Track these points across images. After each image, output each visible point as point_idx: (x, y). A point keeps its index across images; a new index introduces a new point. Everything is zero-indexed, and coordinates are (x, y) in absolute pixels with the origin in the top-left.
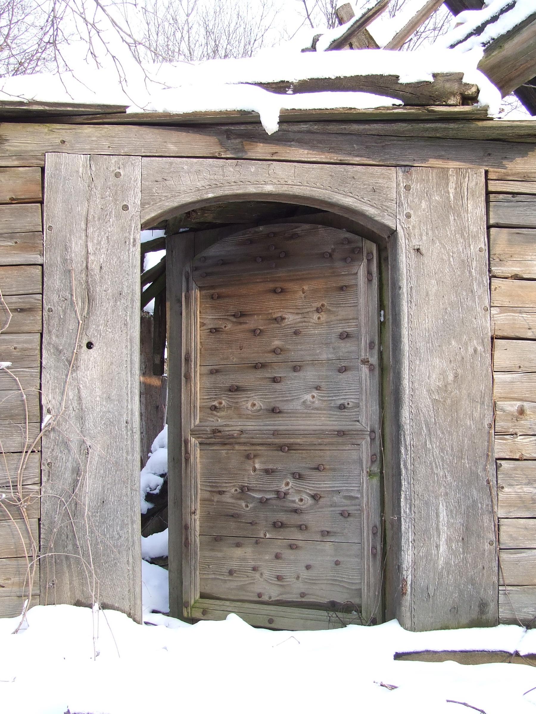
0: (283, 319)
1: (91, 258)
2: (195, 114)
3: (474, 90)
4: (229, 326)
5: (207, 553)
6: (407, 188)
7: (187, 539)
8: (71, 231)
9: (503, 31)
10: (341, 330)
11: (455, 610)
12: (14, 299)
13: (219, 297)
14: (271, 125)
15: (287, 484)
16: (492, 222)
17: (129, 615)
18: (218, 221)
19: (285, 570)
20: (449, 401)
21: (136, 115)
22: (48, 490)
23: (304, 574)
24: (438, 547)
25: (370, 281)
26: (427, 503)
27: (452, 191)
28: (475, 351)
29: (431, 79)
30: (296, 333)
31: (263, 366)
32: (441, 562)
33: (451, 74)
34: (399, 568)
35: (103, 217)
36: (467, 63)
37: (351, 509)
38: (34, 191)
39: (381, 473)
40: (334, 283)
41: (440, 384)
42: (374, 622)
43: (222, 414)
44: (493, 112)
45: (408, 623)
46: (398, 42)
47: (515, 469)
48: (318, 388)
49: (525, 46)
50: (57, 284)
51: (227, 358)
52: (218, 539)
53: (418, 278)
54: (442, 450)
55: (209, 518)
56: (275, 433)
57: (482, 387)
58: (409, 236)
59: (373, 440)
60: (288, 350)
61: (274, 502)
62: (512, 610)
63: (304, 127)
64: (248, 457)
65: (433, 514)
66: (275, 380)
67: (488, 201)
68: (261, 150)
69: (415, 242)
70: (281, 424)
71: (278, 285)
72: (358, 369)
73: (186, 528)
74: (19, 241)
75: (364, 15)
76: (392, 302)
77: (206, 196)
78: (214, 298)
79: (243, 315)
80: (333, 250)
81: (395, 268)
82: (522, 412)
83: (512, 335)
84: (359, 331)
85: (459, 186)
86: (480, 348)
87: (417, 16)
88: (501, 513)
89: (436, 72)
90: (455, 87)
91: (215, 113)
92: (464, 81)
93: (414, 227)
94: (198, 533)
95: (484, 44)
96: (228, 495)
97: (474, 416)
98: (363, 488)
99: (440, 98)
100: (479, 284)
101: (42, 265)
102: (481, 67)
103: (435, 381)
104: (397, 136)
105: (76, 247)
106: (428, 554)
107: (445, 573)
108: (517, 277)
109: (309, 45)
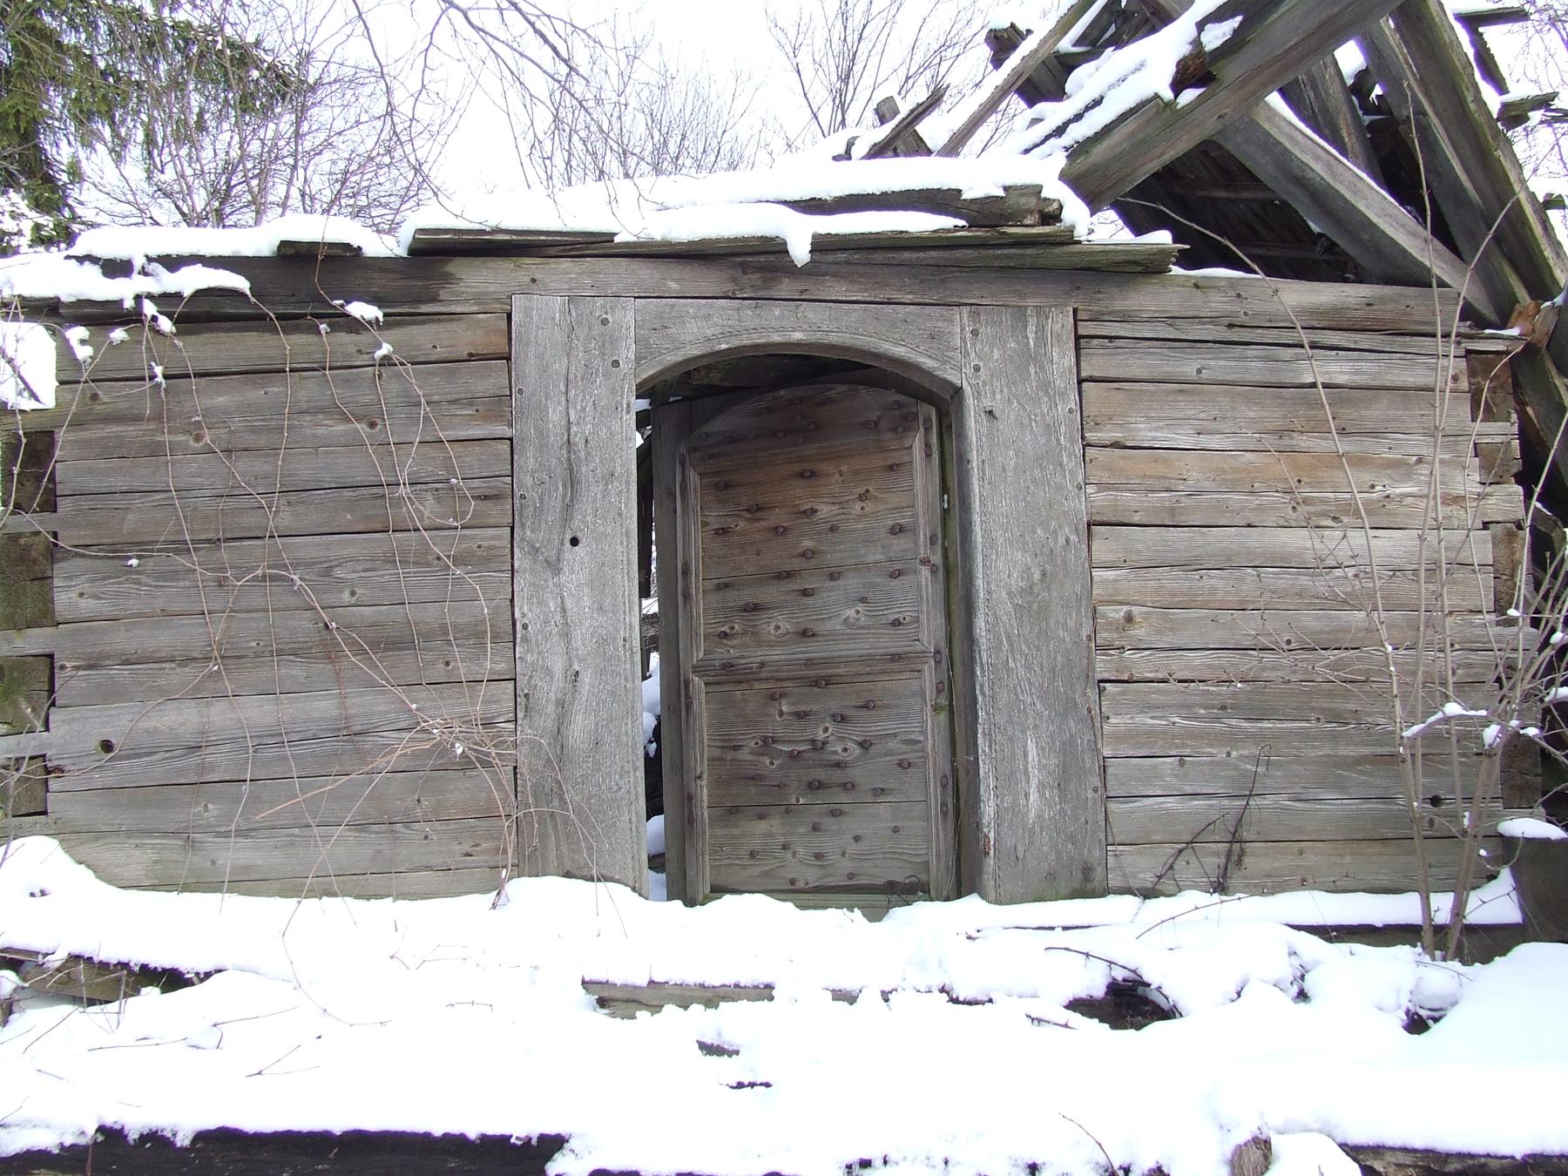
0: (814, 511)
1: (574, 428)
2: (703, 242)
3: (1055, 206)
4: (742, 524)
5: (719, 832)
6: (975, 333)
7: (691, 812)
8: (547, 396)
9: (1090, 133)
10: (890, 523)
11: (1051, 877)
12: (476, 483)
13: (727, 486)
14: (800, 252)
15: (826, 730)
16: (1083, 374)
17: (634, 889)
18: (726, 384)
19: (827, 844)
20: (1035, 606)
21: (627, 244)
22: (526, 732)
23: (852, 848)
24: (1027, 795)
25: (928, 456)
26: (1011, 739)
27: (1031, 336)
28: (1067, 541)
29: (1001, 193)
30: (833, 529)
31: (789, 575)
32: (1032, 815)
33: (1027, 187)
34: (978, 825)
35: (589, 373)
36: (1045, 173)
37: (911, 756)
38: (499, 343)
39: (951, 705)
40: (879, 461)
41: (1023, 584)
42: (947, 899)
43: (736, 642)
44: (1081, 233)
45: (992, 895)
46: (954, 146)
47: (1122, 693)
48: (863, 600)
49: (1119, 149)
50: (531, 463)
51: (741, 568)
52: (733, 811)
53: (991, 449)
54: (1029, 668)
55: (719, 783)
56: (809, 663)
57: (1078, 588)
58: (978, 395)
59: (938, 663)
60: (822, 552)
61: (808, 755)
62: (1124, 876)
63: (842, 256)
64: (772, 698)
65: (1019, 752)
66: (805, 593)
67: (1078, 349)
68: (786, 287)
69: (987, 403)
70: (813, 649)
71: (806, 466)
72: (916, 572)
73: (690, 798)
74: (481, 408)
75: (912, 111)
76: (960, 481)
77: (717, 348)
78: (721, 487)
79: (760, 508)
80: (879, 418)
81: (962, 436)
82: (1129, 618)
83: (1114, 519)
84: (916, 523)
85: (1041, 329)
86: (1073, 538)
87: (979, 111)
88: (1107, 752)
89: (1007, 183)
90: (1033, 202)
91: (729, 240)
92: (1043, 195)
93: (984, 383)
94: (705, 804)
95: (1067, 149)
96: (745, 750)
97: (1069, 625)
98: (930, 729)
99: (1015, 217)
100: (1069, 455)
101: (511, 439)
102: (1064, 177)
103: (1016, 582)
104: (960, 266)
105: (555, 415)
106: (1015, 805)
107: (1037, 829)
108: (1117, 445)
109: (842, 151)
